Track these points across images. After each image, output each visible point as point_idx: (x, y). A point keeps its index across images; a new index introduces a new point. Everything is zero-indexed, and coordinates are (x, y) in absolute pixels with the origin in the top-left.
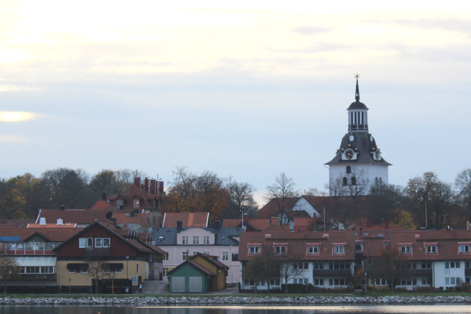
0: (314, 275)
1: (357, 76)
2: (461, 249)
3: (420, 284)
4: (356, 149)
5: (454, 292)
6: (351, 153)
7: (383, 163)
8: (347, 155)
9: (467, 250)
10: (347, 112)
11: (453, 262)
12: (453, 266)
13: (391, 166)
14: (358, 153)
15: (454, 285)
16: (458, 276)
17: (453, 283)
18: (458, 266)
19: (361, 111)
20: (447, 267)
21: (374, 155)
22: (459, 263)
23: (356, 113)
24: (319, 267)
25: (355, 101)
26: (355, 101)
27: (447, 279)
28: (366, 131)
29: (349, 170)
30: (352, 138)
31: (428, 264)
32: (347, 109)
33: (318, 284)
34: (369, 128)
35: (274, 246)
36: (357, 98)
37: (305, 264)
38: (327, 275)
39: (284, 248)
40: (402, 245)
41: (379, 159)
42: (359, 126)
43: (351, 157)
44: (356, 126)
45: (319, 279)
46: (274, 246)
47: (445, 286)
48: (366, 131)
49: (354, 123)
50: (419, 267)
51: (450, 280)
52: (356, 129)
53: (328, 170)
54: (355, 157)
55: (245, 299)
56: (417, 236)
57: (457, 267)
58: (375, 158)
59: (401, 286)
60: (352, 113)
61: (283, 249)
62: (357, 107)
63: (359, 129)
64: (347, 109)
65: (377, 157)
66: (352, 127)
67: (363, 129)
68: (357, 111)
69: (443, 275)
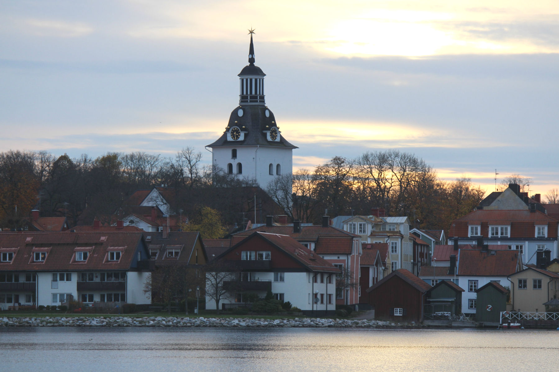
0: (79, 289)
1: (251, 32)
2: (78, 257)
3: (23, 301)
4: (244, 127)
5: (57, 312)
6: (237, 132)
7: (285, 146)
8: (233, 136)
9: (85, 257)
10: (238, 80)
12: (62, 279)
15: (58, 304)
16: (68, 292)
17: (61, 301)
18: (69, 279)
19: (254, 77)
20: (55, 280)
21: (268, 134)
22: (71, 274)
23: (247, 80)
24: (13, 280)
25: (248, 64)
26: (248, 64)
27: (55, 296)
28: (261, 104)
29: (234, 155)
30: (241, 113)
31: (32, 276)
32: (239, 75)
35: (261, 252)
36: (252, 60)
38: (97, 288)
40: (117, 249)
42: (251, 97)
43: (238, 137)
44: (247, 97)
45: (88, 294)
46: (261, 252)
48: (261, 104)
49: (245, 93)
50: (97, 280)
51: (58, 296)
52: (247, 101)
53: (211, 155)
57: (67, 280)
58: (269, 138)
61: (118, 255)
62: (252, 73)
63: (250, 101)
64: (239, 75)
65: (273, 137)
66: (243, 98)
67: (257, 101)
68: (249, 77)
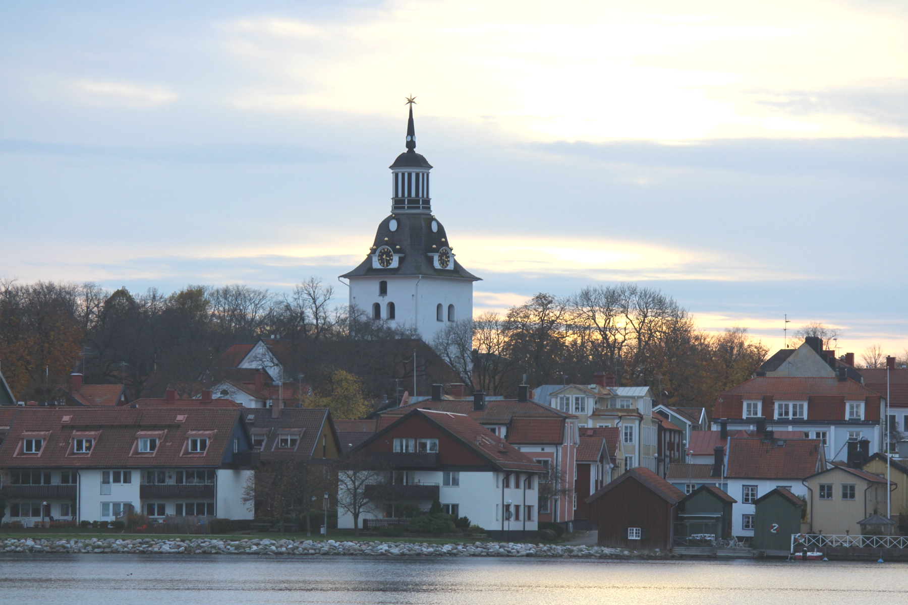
1: (411, 101)
2: (142, 446)
3: (56, 514)
6: (388, 254)
8: (381, 260)
9: (153, 447)
10: (389, 176)
11: (117, 472)
12: (117, 480)
13: (479, 281)
14: (402, 255)
15: (111, 518)
17: (116, 513)
18: (127, 480)
19: (414, 171)
20: (106, 481)
23: (403, 175)
24: (42, 481)
25: (406, 150)
26: (406, 150)
27: (105, 505)
28: (426, 211)
29: (383, 291)
30: (393, 226)
31: (71, 475)
32: (391, 167)
33: (154, 515)
34: (433, 204)
35: (423, 441)
36: (411, 145)
37: (114, 473)
39: (40, 441)
40: (152, 435)
41: (451, 266)
42: (410, 202)
43: (388, 263)
44: (403, 202)
45: (156, 503)
46: (423, 441)
47: (100, 518)
48: (426, 211)
49: (400, 195)
50: (171, 482)
51: (111, 506)
52: (419, 208)
54: (395, 264)
55: (220, 544)
56: (66, 418)
57: (125, 482)
58: (437, 265)
59: (698, 536)
60: (397, 175)
61: (203, 443)
62: (411, 163)
64: (391, 167)
65: (443, 262)
66: (398, 202)
68: (407, 170)
69: (96, 498)
